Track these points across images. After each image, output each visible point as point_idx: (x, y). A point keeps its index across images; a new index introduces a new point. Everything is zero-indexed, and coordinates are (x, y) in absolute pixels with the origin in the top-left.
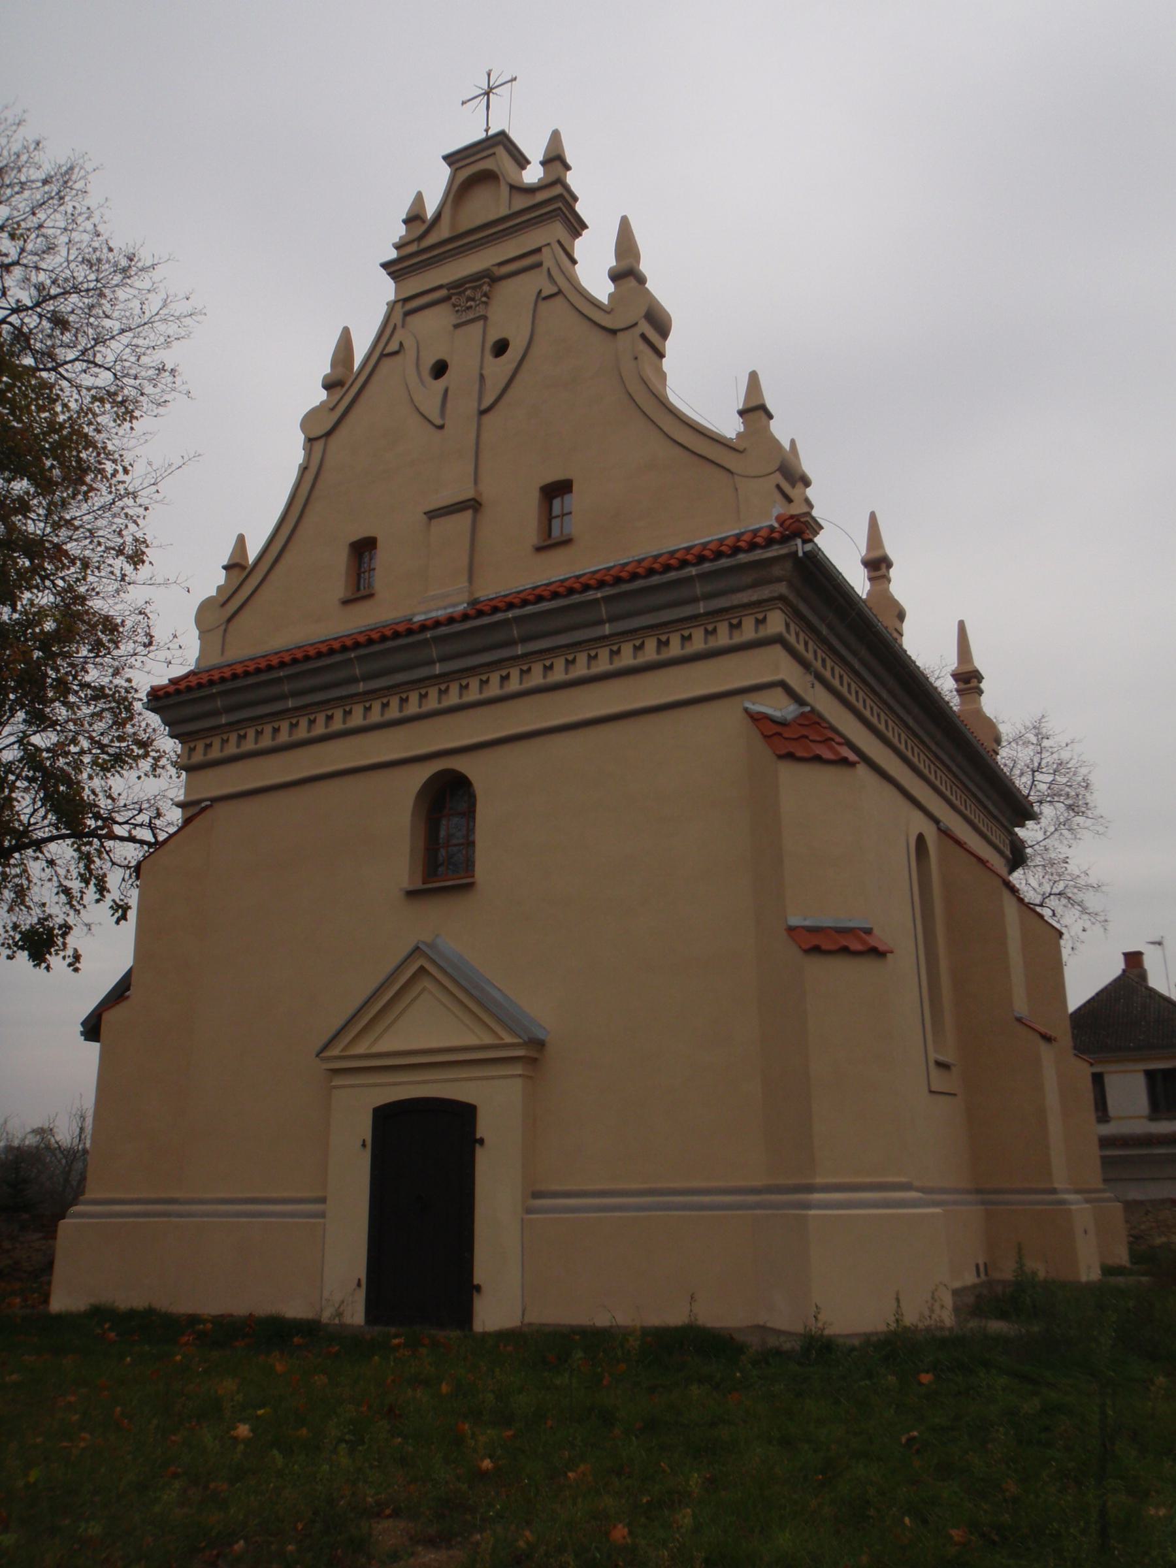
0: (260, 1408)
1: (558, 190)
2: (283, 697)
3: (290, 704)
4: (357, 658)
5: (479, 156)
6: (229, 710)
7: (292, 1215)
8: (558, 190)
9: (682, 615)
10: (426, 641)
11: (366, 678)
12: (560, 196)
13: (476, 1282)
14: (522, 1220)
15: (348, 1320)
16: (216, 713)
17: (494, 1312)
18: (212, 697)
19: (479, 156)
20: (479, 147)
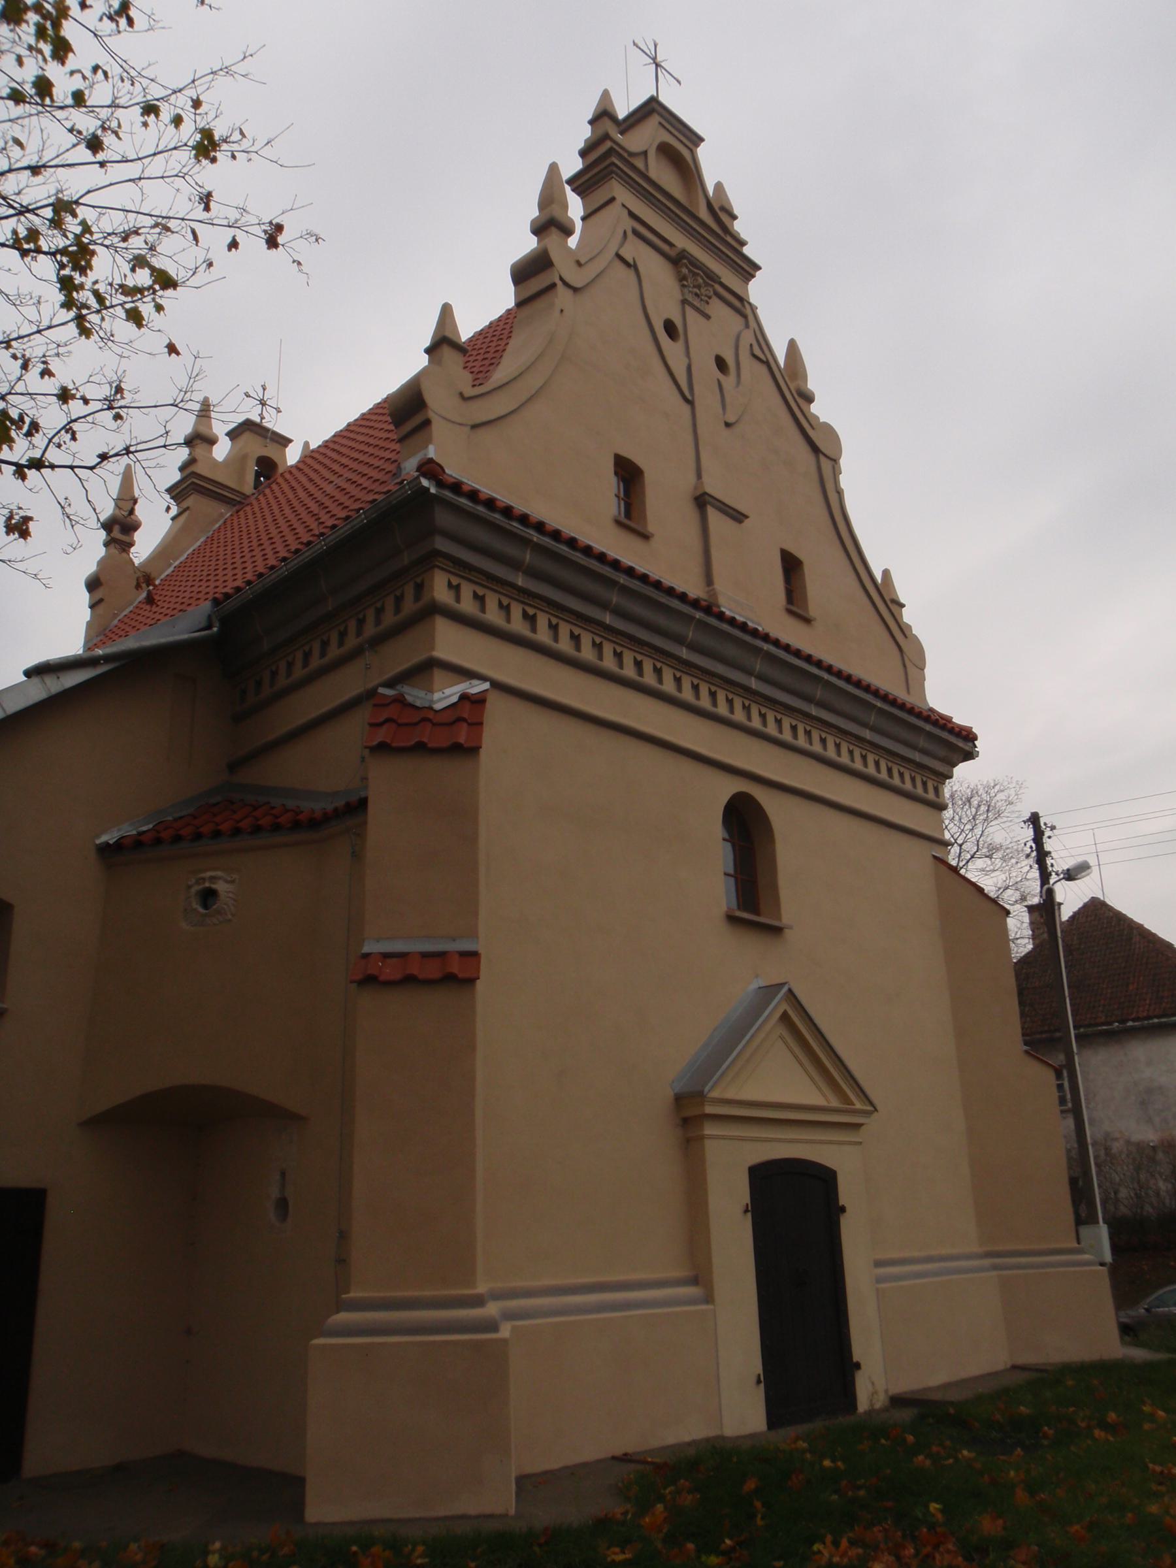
0: (1164, 1410)
1: (608, 144)
2: (605, 606)
3: (608, 619)
4: (880, 709)
5: (676, 133)
6: (533, 573)
7: (918, 1275)
8: (608, 144)
9: (842, 726)
10: (691, 618)
11: (692, 647)
12: (611, 150)
13: (855, 1360)
14: (877, 1290)
15: (731, 1429)
16: (515, 565)
17: (873, 1386)
18: (525, 542)
19: (676, 133)
20: (681, 127)
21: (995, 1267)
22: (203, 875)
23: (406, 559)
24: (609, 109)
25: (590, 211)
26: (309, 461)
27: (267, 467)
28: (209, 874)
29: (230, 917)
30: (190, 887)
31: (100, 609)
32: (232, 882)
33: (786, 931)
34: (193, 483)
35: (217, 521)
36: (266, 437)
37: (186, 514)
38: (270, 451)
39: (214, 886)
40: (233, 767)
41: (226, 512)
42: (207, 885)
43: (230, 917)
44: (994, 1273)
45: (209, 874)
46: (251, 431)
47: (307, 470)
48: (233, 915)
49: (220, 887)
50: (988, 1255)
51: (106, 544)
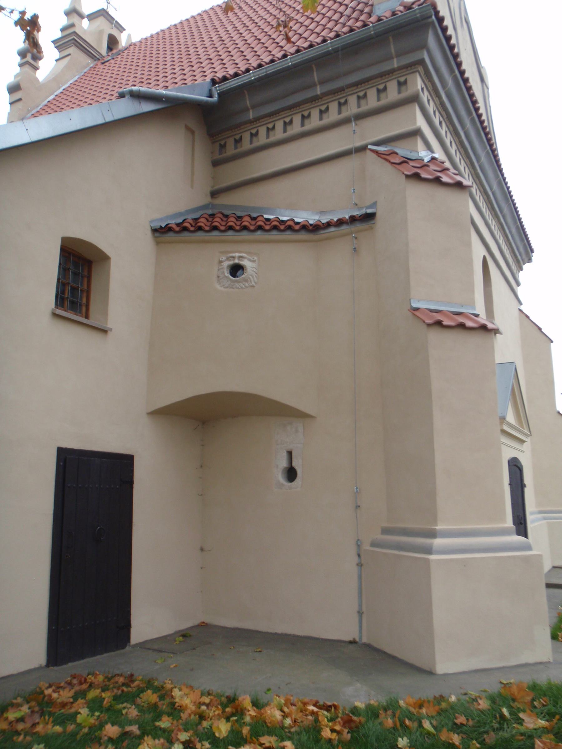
21: (545, 519)
22: (233, 255)
23: (395, 64)
24: (78, 8)
25: (62, 56)
26: (211, 13)
27: (112, 42)
28: (237, 255)
29: (254, 284)
30: (221, 262)
31: (19, 105)
32: (254, 261)
33: (109, 332)
34: (74, 39)
35: (86, 67)
36: (112, 24)
37: (69, 58)
38: (115, 32)
39: (242, 263)
40: (214, 194)
41: (91, 63)
42: (237, 261)
43: (254, 284)
44: (545, 521)
45: (237, 255)
46: (105, 17)
47: (214, 18)
48: (255, 283)
49: (245, 263)
50: (541, 512)
51: (21, 65)
